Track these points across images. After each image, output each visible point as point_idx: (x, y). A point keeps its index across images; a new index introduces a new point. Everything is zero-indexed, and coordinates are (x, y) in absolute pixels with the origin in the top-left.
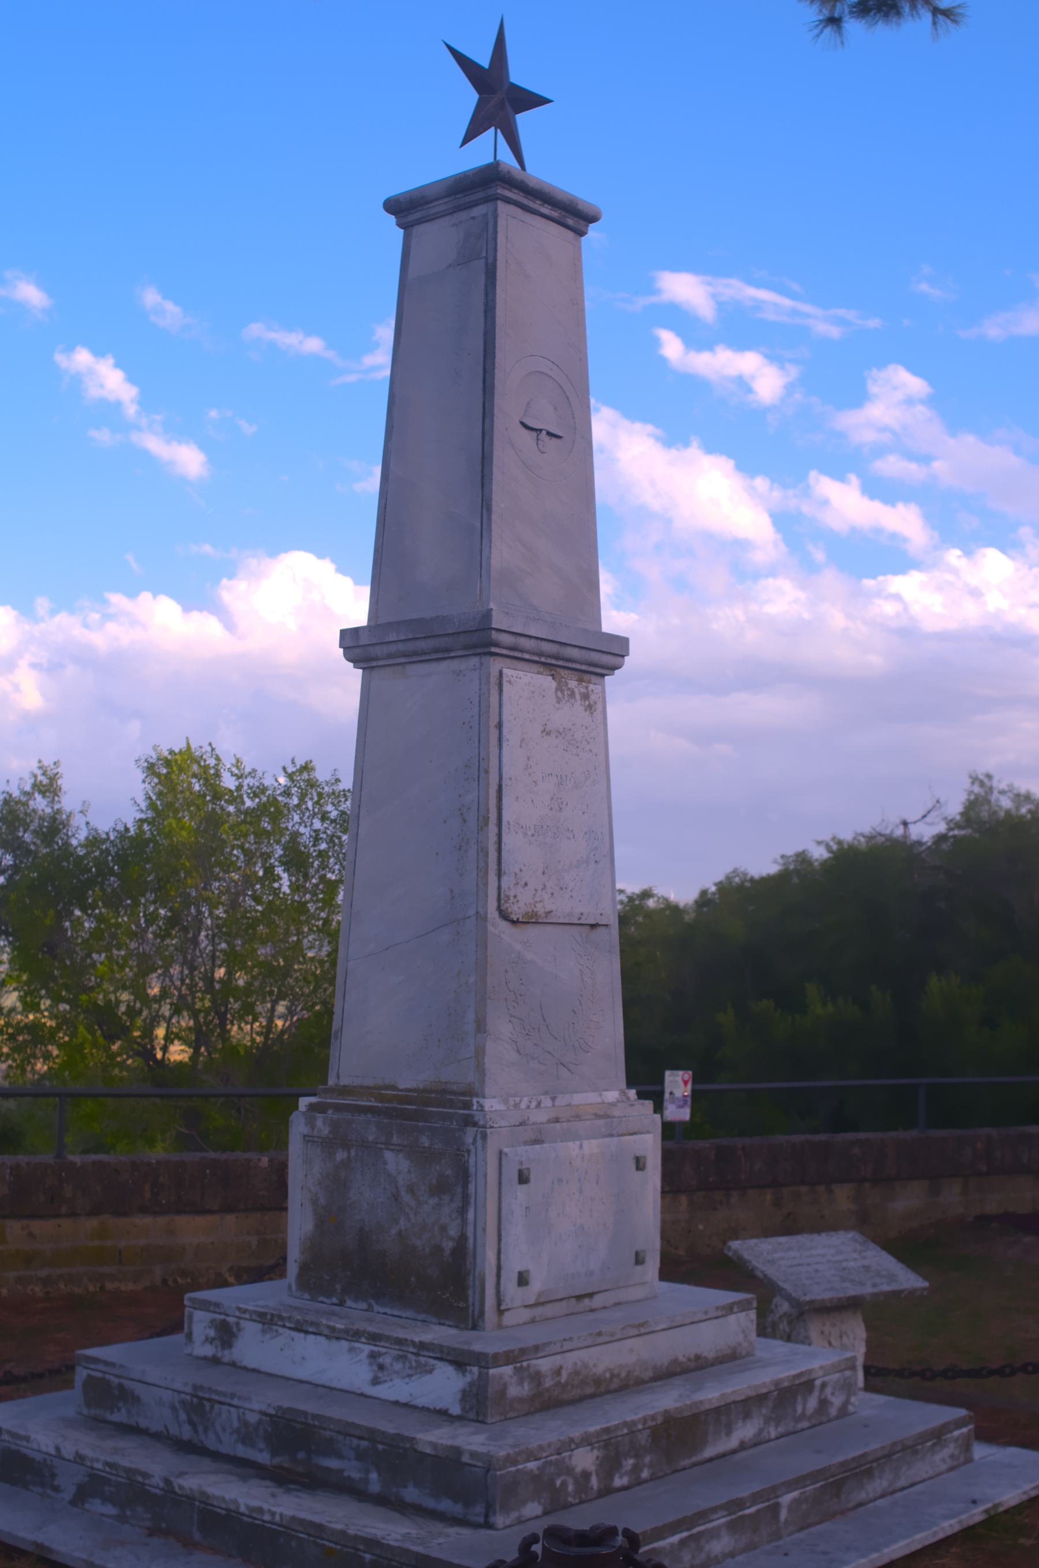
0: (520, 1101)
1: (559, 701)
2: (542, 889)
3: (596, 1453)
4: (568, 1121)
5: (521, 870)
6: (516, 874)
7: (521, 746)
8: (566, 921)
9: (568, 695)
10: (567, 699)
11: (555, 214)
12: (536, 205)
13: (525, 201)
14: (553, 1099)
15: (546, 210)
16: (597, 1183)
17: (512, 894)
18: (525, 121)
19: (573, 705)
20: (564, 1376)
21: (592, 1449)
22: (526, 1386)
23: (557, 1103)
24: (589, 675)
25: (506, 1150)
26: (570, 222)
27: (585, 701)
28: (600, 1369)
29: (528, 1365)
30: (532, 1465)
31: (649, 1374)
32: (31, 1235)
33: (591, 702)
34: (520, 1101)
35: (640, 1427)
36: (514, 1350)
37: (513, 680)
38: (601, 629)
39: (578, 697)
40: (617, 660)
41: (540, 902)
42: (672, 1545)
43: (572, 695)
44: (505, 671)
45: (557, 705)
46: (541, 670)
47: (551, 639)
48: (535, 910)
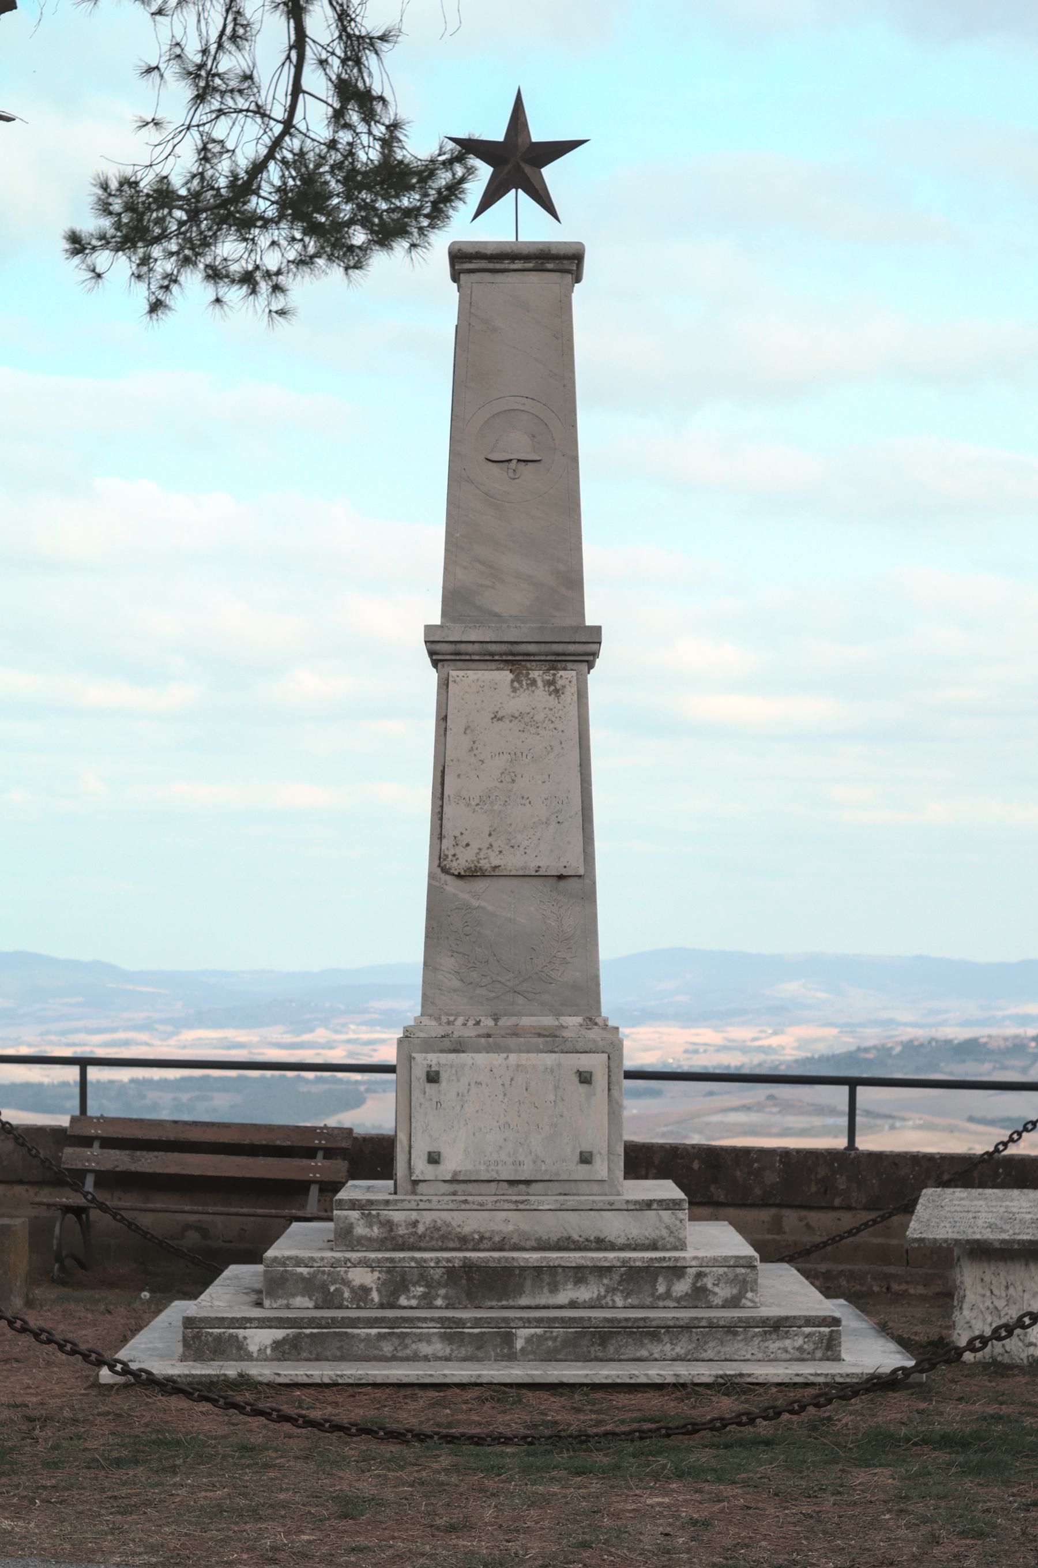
0: (455, 1020)
1: (515, 690)
2: (488, 848)
3: (376, 1274)
4: (503, 1037)
5: (462, 834)
6: (455, 837)
7: (465, 733)
8: (521, 873)
9: (527, 684)
10: (525, 687)
11: (531, 265)
12: (506, 264)
13: (491, 266)
16: (527, 1089)
17: (450, 853)
19: (533, 692)
20: (421, 1229)
21: (372, 1272)
22: (375, 1229)
23: (500, 1023)
24: (564, 663)
26: (550, 266)
27: (549, 687)
28: (467, 1230)
29: (378, 1215)
30: (303, 1270)
32: (808, 1226)
33: (558, 687)
34: (455, 1020)
35: (432, 1264)
36: (362, 1200)
37: (457, 679)
38: (584, 620)
39: (540, 684)
40: (592, 648)
41: (485, 859)
42: (368, 1335)
43: (534, 682)
44: (451, 672)
45: (513, 694)
46: (502, 666)
47: (499, 640)
48: (479, 865)
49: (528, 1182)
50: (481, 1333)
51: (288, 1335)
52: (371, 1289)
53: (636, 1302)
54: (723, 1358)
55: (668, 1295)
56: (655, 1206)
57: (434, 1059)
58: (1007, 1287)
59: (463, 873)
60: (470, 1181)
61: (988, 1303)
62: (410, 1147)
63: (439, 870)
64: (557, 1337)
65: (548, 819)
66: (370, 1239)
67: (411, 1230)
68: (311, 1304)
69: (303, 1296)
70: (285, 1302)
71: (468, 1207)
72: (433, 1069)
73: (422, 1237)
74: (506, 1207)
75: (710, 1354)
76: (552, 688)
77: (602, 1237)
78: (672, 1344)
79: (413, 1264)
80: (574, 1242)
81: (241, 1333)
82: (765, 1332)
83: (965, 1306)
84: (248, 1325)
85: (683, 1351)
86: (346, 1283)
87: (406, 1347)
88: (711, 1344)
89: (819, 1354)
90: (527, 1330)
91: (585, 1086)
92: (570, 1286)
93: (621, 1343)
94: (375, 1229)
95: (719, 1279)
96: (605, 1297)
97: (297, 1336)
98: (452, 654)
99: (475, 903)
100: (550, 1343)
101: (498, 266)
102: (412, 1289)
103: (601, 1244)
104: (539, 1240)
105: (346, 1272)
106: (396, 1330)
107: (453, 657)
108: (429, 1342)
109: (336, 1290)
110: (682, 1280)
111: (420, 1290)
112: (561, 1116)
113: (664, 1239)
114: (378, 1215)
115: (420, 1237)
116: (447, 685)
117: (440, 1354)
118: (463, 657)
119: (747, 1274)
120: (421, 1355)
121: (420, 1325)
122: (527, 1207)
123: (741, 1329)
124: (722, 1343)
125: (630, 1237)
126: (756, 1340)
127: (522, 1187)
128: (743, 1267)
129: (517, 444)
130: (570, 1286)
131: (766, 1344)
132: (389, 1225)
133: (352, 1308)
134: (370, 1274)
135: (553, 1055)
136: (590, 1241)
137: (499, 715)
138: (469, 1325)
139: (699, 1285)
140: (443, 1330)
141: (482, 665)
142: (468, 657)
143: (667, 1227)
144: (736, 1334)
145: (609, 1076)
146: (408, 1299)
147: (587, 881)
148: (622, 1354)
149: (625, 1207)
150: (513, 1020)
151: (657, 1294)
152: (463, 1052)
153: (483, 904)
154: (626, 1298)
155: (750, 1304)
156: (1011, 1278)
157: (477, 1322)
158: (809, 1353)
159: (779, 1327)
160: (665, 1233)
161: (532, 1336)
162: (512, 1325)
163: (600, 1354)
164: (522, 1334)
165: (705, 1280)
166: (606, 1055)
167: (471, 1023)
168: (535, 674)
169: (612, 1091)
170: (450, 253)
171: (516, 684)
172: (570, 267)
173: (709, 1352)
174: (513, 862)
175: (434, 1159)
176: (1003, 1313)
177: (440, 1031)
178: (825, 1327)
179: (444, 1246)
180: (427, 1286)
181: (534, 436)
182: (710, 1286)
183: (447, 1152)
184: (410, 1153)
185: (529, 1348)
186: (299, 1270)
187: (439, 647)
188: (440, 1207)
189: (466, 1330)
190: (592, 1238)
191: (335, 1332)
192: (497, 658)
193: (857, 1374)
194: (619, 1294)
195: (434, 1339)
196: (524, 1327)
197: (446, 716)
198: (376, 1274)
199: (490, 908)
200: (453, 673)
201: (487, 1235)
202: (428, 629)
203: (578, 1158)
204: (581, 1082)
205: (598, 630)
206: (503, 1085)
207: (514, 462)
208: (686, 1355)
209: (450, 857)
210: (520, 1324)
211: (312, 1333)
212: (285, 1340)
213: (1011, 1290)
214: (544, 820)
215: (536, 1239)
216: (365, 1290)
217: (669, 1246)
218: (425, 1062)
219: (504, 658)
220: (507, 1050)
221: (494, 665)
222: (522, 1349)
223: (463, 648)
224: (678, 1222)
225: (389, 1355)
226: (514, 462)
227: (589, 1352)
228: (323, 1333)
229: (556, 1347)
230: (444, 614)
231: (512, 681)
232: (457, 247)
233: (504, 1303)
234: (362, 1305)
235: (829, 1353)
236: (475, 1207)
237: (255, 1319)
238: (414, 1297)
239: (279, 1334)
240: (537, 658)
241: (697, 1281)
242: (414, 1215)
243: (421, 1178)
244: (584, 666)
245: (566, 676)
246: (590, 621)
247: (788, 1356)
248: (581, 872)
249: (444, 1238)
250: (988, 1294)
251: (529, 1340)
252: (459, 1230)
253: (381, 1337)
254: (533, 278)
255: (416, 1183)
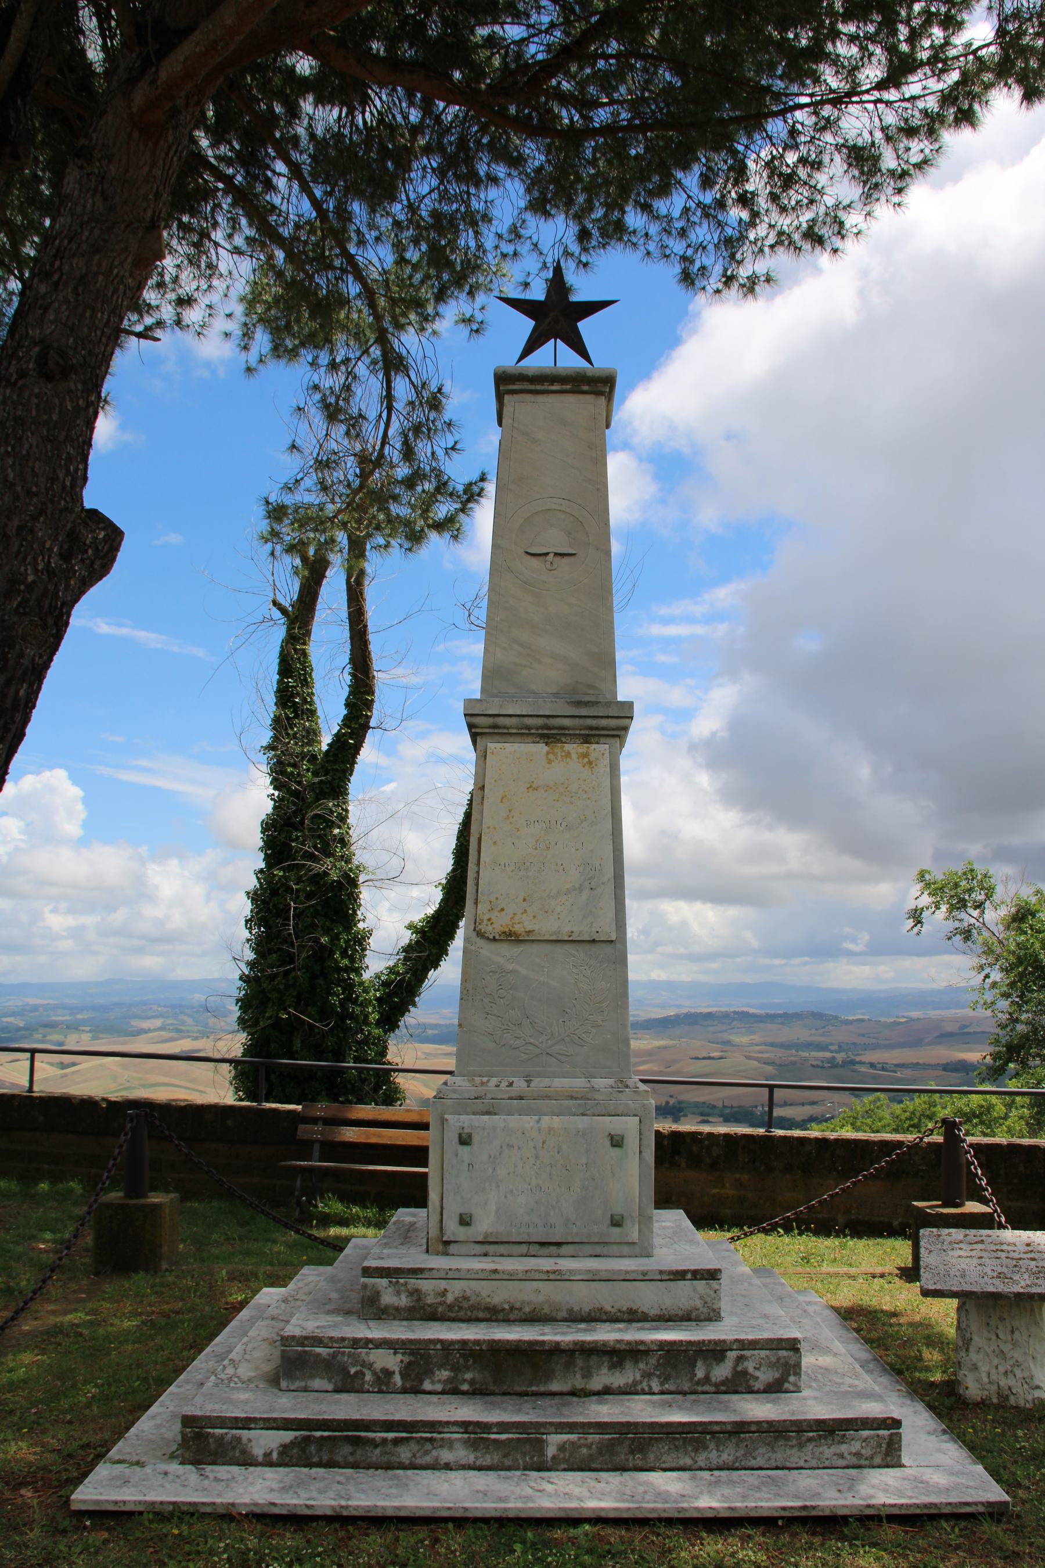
1: (550, 762)
8: (554, 938)
10: (559, 758)
11: (568, 387)
13: (532, 387)
14: (529, 1082)
15: (556, 387)
17: (485, 918)
18: (586, 327)
21: (395, 1353)
25: (446, 1116)
29: (406, 1283)
31: (563, 1314)
33: (591, 759)
39: (574, 756)
40: (626, 721)
43: (568, 754)
45: (548, 766)
49: (558, 1244)
50: (508, 1439)
51: (296, 1438)
52: (393, 1373)
53: (673, 1388)
54: (774, 1465)
55: (707, 1379)
56: (689, 1276)
57: (466, 1120)
58: (1012, 1332)
59: (497, 937)
60: (502, 1243)
61: (994, 1346)
62: (442, 1208)
63: (474, 934)
64: (592, 1444)
65: (581, 885)
66: (397, 1309)
67: (439, 1300)
68: (330, 1387)
69: (322, 1378)
70: (303, 1384)
71: (496, 1276)
72: (466, 1131)
73: (450, 1307)
74: (537, 1277)
75: (760, 1461)
76: (586, 760)
77: (635, 1308)
78: (718, 1451)
79: (439, 1346)
80: (606, 1313)
81: (245, 1434)
82: (820, 1437)
83: (971, 1349)
84: (253, 1426)
85: (731, 1458)
86: (370, 1366)
87: (427, 1453)
88: (762, 1450)
89: (878, 1460)
90: (559, 1436)
91: (617, 1149)
92: (604, 1370)
93: (662, 1451)
94: (403, 1297)
95: (761, 1364)
96: (641, 1382)
97: (307, 1439)
98: (490, 727)
99: (510, 967)
100: (584, 1451)
101: (539, 387)
102: (437, 1372)
103: (633, 1317)
104: (571, 1311)
105: (367, 1354)
106: (414, 1435)
107: (492, 731)
108: (451, 1448)
109: (356, 1372)
110: (722, 1364)
111: (445, 1374)
112: (593, 1179)
113: (698, 1309)
114: (406, 1283)
115: (449, 1306)
116: (485, 757)
117: (463, 1462)
118: (501, 731)
119: (790, 1357)
120: (442, 1462)
121: (441, 1429)
122: (559, 1277)
123: (794, 1434)
124: (772, 1448)
125: (664, 1308)
126: (810, 1446)
127: (553, 1249)
128: (786, 1349)
129: (554, 540)
130: (604, 1370)
131: (821, 1449)
132: (416, 1293)
133: (373, 1392)
134: (392, 1356)
135: (585, 1118)
136: (623, 1312)
137: (534, 786)
138: (495, 1430)
139: (739, 1369)
140: (466, 1436)
141: (519, 739)
142: (505, 731)
143: (701, 1298)
144: (788, 1439)
145: (640, 1139)
146: (433, 1383)
147: (618, 946)
148: (664, 1462)
149: (659, 1277)
150: (546, 1081)
151: (696, 1379)
152: (495, 1114)
153: (518, 968)
154: (662, 1384)
155: (792, 1388)
156: (1016, 1324)
157: (503, 1427)
158: (866, 1459)
159: (834, 1431)
160: (698, 1303)
161: (565, 1443)
162: (542, 1430)
163: (640, 1463)
164: (554, 1441)
165: (746, 1364)
166: (637, 1118)
167: (504, 1084)
168: (568, 747)
169: (644, 1154)
170: (495, 375)
171: (551, 756)
172: (603, 389)
173: (759, 1459)
174: (546, 927)
175: (465, 1221)
176: (1008, 1356)
177: (474, 1091)
178: (884, 1429)
179: (473, 1317)
180: (452, 1370)
181: (570, 533)
182: (751, 1370)
183: (478, 1213)
184: (442, 1214)
185: (562, 1456)
186: (318, 1350)
187: (477, 720)
188: (468, 1276)
189: (493, 1436)
190: (625, 1309)
191: (347, 1436)
192: (533, 731)
193: (935, 1505)
194: (656, 1379)
195: (457, 1445)
196: (557, 1433)
197: (484, 786)
198: (399, 1357)
199: (523, 971)
200: (491, 746)
201: (518, 1305)
202: (468, 702)
203: (609, 1222)
204: (613, 1145)
205: (630, 705)
206: (535, 1148)
207: (552, 555)
208: (734, 1462)
209: (485, 922)
210: (552, 1429)
211: (322, 1436)
212: (293, 1443)
213: (1017, 1335)
214: (577, 886)
215: (568, 1310)
216: (388, 1373)
217: (702, 1317)
218: (458, 1124)
219: (540, 731)
220: (540, 1113)
221: (530, 739)
222: (554, 1457)
223: (501, 721)
224: (712, 1293)
225: (407, 1462)
226: (552, 555)
227: (627, 1460)
228: (335, 1437)
229: (591, 1455)
230: (483, 690)
231: (548, 753)
232: (501, 371)
233: (534, 1388)
234: (384, 1388)
235: (889, 1459)
236: (505, 1277)
237: (261, 1419)
238: (439, 1381)
239: (288, 1436)
240: (571, 732)
241: (737, 1365)
242: (443, 1284)
243: (452, 1239)
244: (616, 742)
245: (599, 750)
246: (623, 695)
247: (841, 1462)
248: (613, 937)
249: (472, 1308)
250: (994, 1338)
251: (562, 1448)
252: (488, 1300)
253: (397, 1442)
254: (571, 399)
255: (447, 1243)
